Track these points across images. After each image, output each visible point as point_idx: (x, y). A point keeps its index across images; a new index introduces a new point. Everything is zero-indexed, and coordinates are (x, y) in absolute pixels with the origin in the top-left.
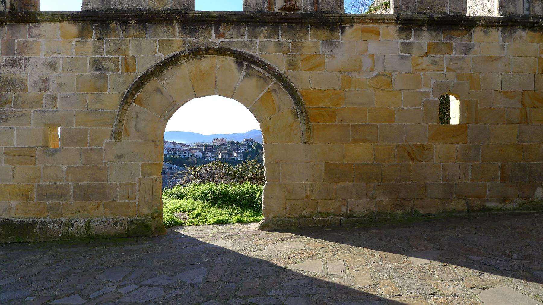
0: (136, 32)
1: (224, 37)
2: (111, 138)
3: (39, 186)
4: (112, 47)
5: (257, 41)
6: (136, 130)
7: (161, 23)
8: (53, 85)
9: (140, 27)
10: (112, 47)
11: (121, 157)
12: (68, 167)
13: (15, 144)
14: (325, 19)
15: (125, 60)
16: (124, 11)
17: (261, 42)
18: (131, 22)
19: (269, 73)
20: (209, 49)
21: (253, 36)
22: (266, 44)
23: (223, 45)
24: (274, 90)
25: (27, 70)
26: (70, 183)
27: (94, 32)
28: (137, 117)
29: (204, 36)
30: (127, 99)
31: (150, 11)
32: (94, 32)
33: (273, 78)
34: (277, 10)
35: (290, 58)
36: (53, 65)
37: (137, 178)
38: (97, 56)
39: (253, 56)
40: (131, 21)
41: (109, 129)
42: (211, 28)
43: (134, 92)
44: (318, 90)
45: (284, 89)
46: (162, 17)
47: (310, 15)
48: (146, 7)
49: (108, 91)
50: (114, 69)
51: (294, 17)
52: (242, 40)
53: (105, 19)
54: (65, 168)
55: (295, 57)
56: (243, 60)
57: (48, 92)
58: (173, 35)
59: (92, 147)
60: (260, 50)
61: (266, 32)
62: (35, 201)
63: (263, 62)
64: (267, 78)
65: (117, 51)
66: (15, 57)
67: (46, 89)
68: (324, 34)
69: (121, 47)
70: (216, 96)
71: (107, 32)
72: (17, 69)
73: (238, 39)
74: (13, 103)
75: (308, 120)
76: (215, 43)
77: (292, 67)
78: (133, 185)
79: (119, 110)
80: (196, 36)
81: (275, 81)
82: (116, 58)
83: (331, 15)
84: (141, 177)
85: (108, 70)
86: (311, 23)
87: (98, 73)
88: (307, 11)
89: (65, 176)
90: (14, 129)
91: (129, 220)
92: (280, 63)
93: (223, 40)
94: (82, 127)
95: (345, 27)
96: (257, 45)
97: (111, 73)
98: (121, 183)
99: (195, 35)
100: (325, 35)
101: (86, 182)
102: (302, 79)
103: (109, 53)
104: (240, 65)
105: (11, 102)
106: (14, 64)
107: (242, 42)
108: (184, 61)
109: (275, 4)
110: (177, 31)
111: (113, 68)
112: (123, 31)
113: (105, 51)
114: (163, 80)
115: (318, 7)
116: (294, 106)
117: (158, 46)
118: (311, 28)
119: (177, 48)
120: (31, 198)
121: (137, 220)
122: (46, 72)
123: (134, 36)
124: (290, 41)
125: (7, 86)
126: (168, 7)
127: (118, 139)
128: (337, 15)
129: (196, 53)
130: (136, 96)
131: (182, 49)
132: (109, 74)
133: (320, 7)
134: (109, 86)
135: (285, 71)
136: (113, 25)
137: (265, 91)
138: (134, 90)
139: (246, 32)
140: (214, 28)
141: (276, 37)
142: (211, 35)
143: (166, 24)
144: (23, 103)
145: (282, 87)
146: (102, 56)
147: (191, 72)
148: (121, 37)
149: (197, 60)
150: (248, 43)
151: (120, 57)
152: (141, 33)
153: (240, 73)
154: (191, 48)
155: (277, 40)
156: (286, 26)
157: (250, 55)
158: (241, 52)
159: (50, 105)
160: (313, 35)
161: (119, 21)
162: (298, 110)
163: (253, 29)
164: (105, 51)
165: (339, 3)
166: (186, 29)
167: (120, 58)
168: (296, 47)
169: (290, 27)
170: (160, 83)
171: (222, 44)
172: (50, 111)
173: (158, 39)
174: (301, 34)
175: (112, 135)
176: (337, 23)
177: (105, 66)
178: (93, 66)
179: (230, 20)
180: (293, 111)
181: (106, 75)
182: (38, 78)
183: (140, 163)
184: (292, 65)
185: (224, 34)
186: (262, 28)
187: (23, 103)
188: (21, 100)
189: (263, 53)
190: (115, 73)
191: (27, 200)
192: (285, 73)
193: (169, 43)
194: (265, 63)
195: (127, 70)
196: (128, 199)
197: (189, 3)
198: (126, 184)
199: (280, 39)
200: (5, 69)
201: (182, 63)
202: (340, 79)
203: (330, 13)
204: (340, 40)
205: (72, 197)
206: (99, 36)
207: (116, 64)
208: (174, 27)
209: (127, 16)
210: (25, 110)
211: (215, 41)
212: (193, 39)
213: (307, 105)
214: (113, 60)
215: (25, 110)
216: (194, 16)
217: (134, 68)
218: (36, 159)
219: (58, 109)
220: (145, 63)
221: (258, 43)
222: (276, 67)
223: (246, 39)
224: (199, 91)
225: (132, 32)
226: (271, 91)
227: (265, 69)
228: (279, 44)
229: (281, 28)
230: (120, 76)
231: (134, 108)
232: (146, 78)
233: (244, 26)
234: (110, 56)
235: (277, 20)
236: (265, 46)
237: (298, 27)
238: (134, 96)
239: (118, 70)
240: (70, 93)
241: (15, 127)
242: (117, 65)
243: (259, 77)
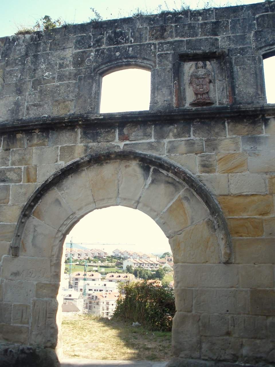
0: (40, 140)
1: (128, 140)
4: (17, 157)
5: (166, 141)
6: (33, 245)
7: (64, 129)
9: (43, 135)
10: (17, 157)
11: (16, 274)
14: (244, 112)
16: (30, 121)
17: (170, 142)
18: (36, 131)
19: (180, 178)
20: (111, 154)
21: (161, 136)
22: (175, 144)
23: (128, 149)
24: (186, 198)
27: (2, 144)
28: (35, 231)
29: (107, 139)
30: (28, 211)
31: (53, 119)
32: (2, 144)
33: (184, 183)
34: (187, 106)
35: (204, 158)
37: (32, 299)
38: (3, 167)
39: (160, 159)
40: (35, 129)
42: (115, 130)
43: (32, 204)
44: (240, 196)
45: (198, 197)
46: (64, 123)
47: (226, 108)
48: (50, 114)
49: (10, 203)
50: (17, 180)
51: (207, 112)
52: (148, 141)
53: (12, 130)
55: (210, 157)
56: (149, 164)
58: (75, 141)
60: (169, 151)
61: (175, 130)
63: (171, 165)
64: (177, 184)
65: (20, 162)
68: (244, 128)
70: (120, 207)
71: (13, 143)
73: (143, 142)
75: (227, 234)
76: (118, 147)
77: (207, 169)
78: (27, 307)
79: (18, 223)
80: (99, 140)
81: (187, 186)
82: (19, 168)
83: (249, 106)
84: (35, 298)
86: (228, 118)
88: (223, 104)
91: (21, 348)
92: (191, 165)
93: (127, 142)
95: (269, 119)
96: (165, 146)
97: (13, 184)
98: (15, 303)
99: (97, 139)
100: (245, 130)
102: (217, 182)
103: (13, 164)
104: (146, 169)
107: (149, 143)
108: (85, 168)
109: (185, 99)
110: (80, 136)
111: (16, 179)
112: (28, 140)
113: (10, 162)
115: (235, 99)
116: (210, 217)
117: (59, 154)
118: (228, 123)
119: (79, 153)
121: (29, 349)
123: (37, 145)
124: (204, 138)
126: (72, 112)
127: (16, 255)
128: (258, 105)
129: (97, 160)
130: (35, 208)
131: (83, 156)
132: (11, 184)
133: (238, 98)
134: (10, 198)
135: (199, 174)
136: (19, 136)
137: (174, 200)
138: (32, 201)
139: (153, 133)
140: (117, 130)
141: (187, 136)
142: (113, 139)
143: (68, 130)
145: (195, 193)
146: (7, 167)
147: (92, 180)
148: (26, 147)
149: (99, 167)
150: (155, 145)
151: (23, 167)
152: (44, 141)
153: (146, 178)
154: (92, 154)
155: (189, 138)
156: (199, 122)
157: (156, 158)
158: (145, 155)
160: (231, 131)
161: (24, 131)
162: (215, 222)
163: (161, 128)
164: (10, 162)
165: (259, 92)
166: (88, 133)
167: (23, 168)
168: (212, 145)
169: (203, 123)
170: (60, 193)
171: (125, 147)
173: (60, 146)
174: (217, 130)
175: (9, 250)
176: (259, 115)
177: (9, 177)
179: (135, 120)
180: (209, 223)
181: (9, 186)
183: (35, 283)
184: (207, 167)
185: (129, 136)
186: (171, 127)
189: (173, 155)
190: (17, 184)
192: (199, 176)
193: (71, 150)
194: (174, 166)
196: (21, 322)
197: (92, 107)
198: (20, 305)
199: (192, 137)
201: (82, 170)
202: (267, 181)
203: (249, 104)
204: (264, 134)
206: (5, 147)
207: (18, 175)
208: (76, 132)
209: (32, 125)
211: (119, 145)
212: (95, 144)
213: (228, 216)
214: (16, 171)
216: (96, 119)
217: (35, 178)
220: (46, 172)
221: (166, 144)
222: (187, 170)
223: (153, 140)
224: (99, 202)
225: (35, 141)
226: (182, 199)
227: (175, 173)
228: (191, 144)
229: (193, 125)
231: (33, 221)
232: (45, 188)
233: (150, 126)
234: (14, 167)
235: (187, 117)
236: (175, 148)
237: (213, 123)
238: (32, 209)
239: (20, 181)
243: (168, 183)
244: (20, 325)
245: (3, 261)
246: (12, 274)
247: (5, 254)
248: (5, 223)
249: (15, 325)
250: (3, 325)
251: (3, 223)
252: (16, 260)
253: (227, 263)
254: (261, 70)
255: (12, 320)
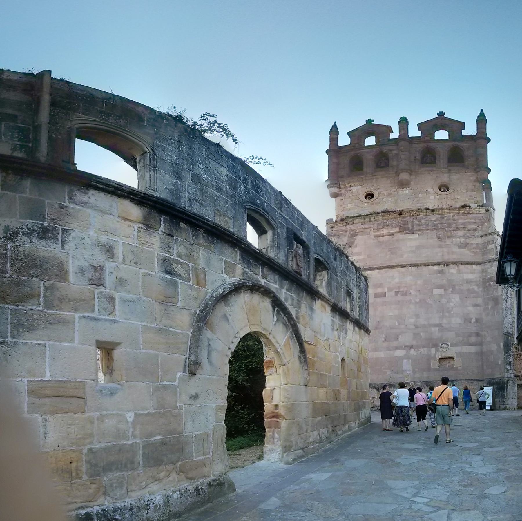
2: (184, 371)
3: (90, 450)
8: (109, 280)
11: (195, 397)
12: (136, 414)
13: (48, 374)
15: (195, 270)
25: (67, 247)
26: (138, 441)
27: (162, 225)
28: (209, 345)
36: (109, 251)
37: (212, 425)
41: (181, 358)
45: (295, 338)
49: (179, 304)
54: (130, 417)
57: (102, 289)
59: (165, 383)
62: (85, 477)
66: (46, 224)
67: (99, 283)
69: (192, 254)
72: (50, 243)
74: (41, 299)
78: (208, 435)
85: (179, 276)
87: (168, 276)
89: (131, 430)
90: (45, 346)
94: (151, 351)
101: (158, 437)
105: (39, 296)
106: (45, 233)
112: (193, 236)
114: (229, 306)
120: (77, 474)
122: (100, 258)
123: (203, 246)
125: (29, 266)
127: (193, 374)
132: (180, 281)
136: (183, 225)
144: (61, 300)
152: (210, 246)
159: (105, 309)
172: (106, 320)
177: (176, 270)
178: (162, 266)
182: (87, 264)
183: (214, 406)
187: (61, 300)
188: (58, 294)
190: (186, 283)
191: (71, 478)
195: (198, 284)
196: (204, 454)
198: (201, 434)
200: (25, 238)
205: (141, 463)
210: (65, 314)
215: (65, 314)
218: (85, 403)
219: (117, 318)
230: (191, 287)
240: (134, 297)
241: (48, 343)
242: (187, 272)
244: (202, 458)
245: (179, 381)
246: (190, 398)
247: (180, 372)
248: (177, 331)
249: (197, 459)
250: (187, 462)
251: (174, 330)
252: (194, 379)
253: (306, 386)
254: (449, 136)
255: (194, 454)
